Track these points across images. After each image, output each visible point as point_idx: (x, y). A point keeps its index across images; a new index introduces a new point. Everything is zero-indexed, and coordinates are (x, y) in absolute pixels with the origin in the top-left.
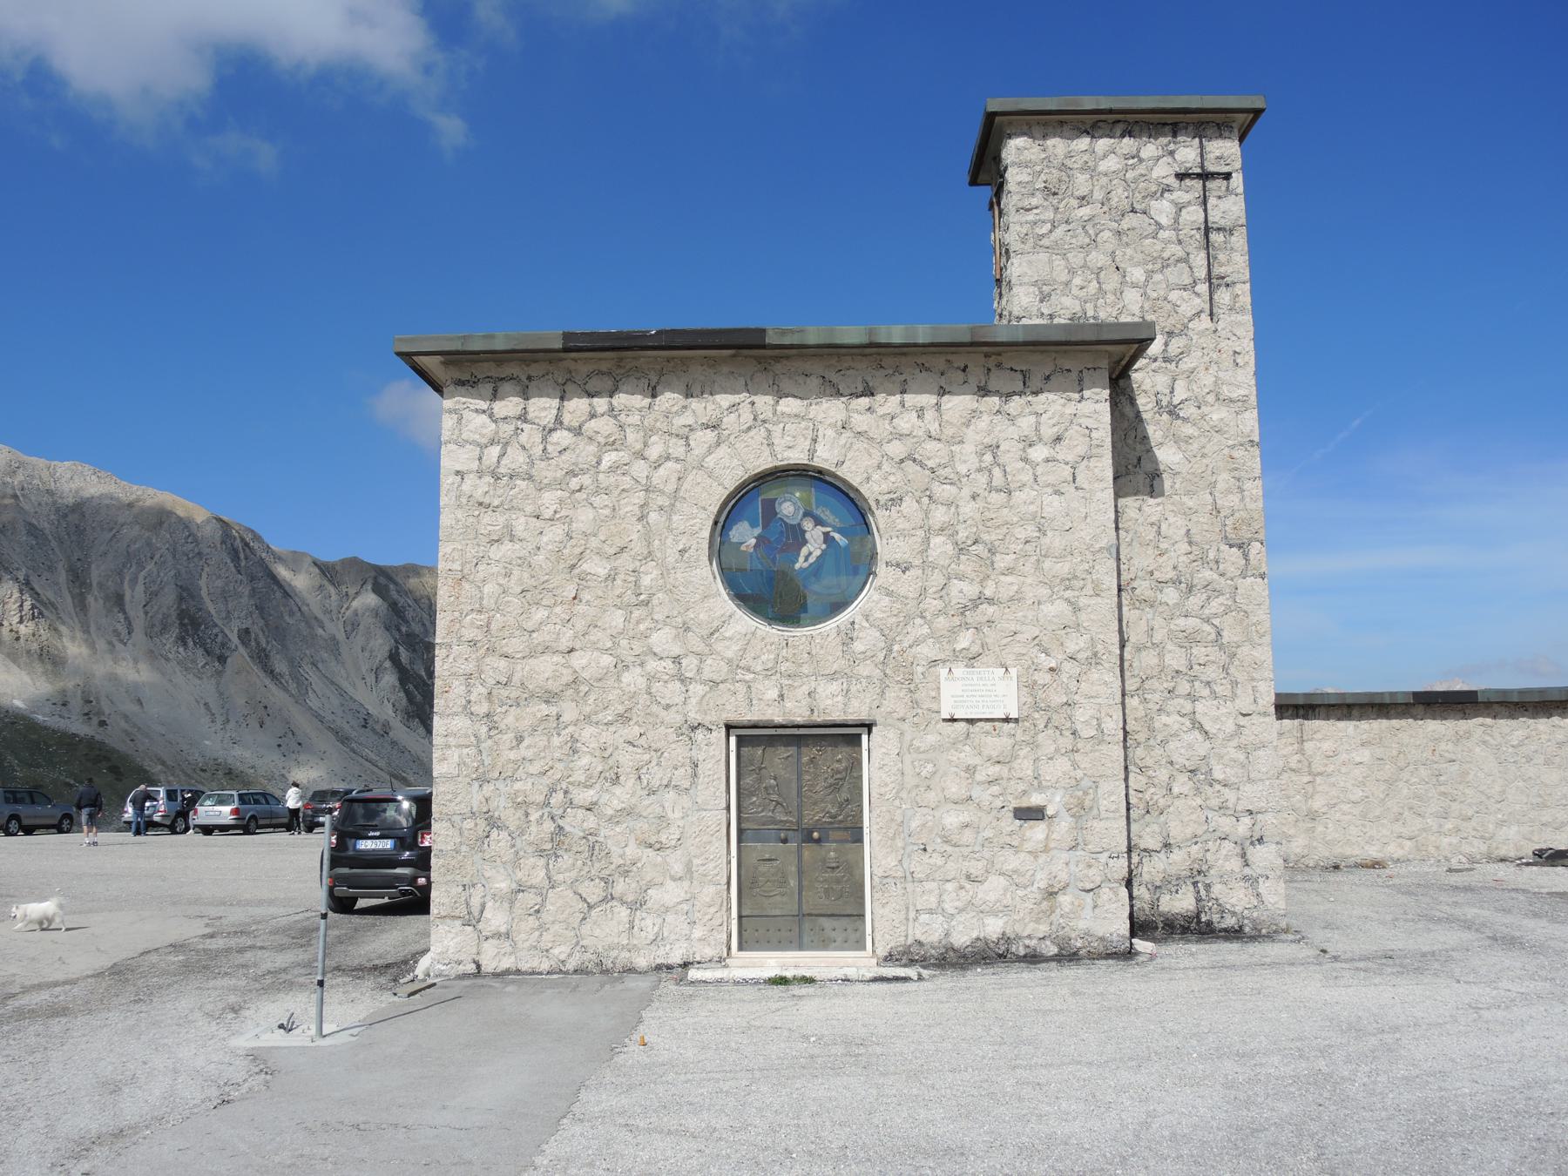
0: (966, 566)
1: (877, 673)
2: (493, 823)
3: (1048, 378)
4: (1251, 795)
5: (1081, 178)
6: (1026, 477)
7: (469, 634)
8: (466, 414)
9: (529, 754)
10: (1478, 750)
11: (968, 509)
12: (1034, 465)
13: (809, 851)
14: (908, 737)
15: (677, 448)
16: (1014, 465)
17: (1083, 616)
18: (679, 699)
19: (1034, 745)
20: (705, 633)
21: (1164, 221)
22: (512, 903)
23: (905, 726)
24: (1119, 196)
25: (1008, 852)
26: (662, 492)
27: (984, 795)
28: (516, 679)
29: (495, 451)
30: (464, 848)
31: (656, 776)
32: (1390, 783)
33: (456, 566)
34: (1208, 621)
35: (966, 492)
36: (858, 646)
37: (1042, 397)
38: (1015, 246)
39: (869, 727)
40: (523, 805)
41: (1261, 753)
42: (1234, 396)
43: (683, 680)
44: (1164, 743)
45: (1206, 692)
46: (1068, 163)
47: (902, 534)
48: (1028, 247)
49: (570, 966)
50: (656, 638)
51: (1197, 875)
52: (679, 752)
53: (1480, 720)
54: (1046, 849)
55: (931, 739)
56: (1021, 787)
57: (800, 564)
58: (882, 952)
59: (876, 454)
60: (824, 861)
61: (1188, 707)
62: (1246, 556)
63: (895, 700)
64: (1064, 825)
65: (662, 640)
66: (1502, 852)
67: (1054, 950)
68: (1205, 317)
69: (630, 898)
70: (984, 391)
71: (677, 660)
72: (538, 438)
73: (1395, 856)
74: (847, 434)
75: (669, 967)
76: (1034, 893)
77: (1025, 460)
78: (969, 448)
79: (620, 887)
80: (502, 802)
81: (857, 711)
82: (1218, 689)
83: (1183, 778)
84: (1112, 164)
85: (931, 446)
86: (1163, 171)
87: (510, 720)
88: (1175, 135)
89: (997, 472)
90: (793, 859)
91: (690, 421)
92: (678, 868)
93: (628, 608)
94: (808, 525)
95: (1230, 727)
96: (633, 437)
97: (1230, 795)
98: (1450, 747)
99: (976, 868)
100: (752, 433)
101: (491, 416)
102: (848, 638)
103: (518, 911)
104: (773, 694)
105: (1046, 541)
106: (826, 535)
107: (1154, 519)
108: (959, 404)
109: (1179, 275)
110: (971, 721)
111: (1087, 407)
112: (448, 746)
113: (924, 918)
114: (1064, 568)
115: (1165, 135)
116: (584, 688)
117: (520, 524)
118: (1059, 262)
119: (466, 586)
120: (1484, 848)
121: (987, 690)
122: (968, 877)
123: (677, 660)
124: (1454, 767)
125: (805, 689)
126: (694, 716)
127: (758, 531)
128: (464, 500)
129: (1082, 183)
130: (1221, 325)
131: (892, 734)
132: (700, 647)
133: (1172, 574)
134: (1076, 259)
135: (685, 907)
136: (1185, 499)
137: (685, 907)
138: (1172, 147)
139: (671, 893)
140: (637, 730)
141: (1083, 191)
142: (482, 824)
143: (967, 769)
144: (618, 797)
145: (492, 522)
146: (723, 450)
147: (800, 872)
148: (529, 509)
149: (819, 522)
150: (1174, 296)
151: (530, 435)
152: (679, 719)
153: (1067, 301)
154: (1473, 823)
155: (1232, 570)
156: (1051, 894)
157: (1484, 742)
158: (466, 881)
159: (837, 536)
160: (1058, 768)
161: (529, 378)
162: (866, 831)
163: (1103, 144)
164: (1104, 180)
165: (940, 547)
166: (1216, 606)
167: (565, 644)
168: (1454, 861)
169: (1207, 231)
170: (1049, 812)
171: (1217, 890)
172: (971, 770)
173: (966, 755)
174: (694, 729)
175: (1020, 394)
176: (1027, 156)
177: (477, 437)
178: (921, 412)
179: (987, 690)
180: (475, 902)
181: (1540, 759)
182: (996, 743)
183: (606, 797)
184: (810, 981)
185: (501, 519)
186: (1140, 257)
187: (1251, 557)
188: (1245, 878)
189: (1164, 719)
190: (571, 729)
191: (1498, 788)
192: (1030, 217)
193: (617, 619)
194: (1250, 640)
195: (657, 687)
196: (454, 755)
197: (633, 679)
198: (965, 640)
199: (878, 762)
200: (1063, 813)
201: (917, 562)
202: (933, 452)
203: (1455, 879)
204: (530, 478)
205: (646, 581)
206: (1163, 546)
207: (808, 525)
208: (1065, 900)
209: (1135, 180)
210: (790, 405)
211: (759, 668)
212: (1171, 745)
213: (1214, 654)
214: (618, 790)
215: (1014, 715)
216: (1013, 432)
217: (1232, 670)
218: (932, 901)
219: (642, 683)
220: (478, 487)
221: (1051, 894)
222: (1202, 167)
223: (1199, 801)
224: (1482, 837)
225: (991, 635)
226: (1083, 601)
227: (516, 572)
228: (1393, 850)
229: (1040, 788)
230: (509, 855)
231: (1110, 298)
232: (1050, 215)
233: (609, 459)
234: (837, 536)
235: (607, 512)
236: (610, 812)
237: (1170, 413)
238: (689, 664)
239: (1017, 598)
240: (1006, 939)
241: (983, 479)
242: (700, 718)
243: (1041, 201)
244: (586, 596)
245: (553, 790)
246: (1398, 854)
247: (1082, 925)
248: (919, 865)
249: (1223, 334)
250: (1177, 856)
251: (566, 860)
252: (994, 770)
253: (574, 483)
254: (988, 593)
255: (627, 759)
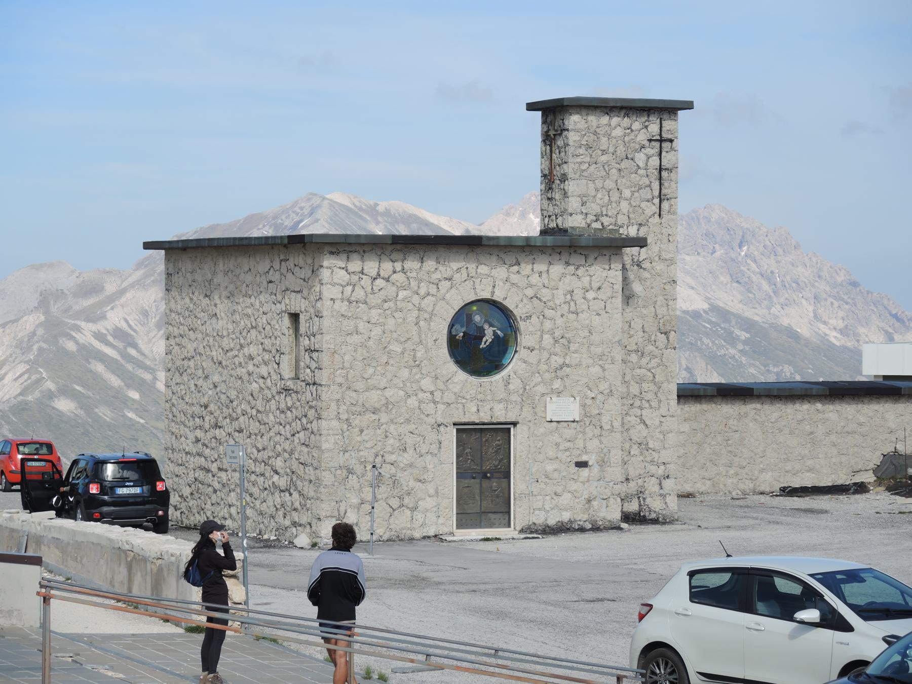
0: (558, 349)
1: (519, 399)
2: (350, 471)
3: (596, 259)
4: (665, 456)
5: (604, 140)
6: (585, 307)
7: (339, 380)
8: (335, 269)
9: (366, 438)
10: (751, 424)
11: (560, 321)
12: (588, 301)
13: (486, 483)
14: (532, 430)
15: (433, 290)
16: (580, 301)
17: (606, 373)
18: (433, 412)
19: (584, 433)
20: (445, 380)
21: (641, 165)
22: (358, 509)
23: (531, 424)
24: (621, 150)
25: (572, 482)
26: (426, 311)
27: (563, 456)
28: (360, 403)
29: (350, 288)
30: (336, 484)
31: (424, 448)
32: (700, 445)
33: (332, 346)
34: (649, 370)
35: (559, 313)
36: (511, 387)
37: (593, 268)
38: (571, 175)
39: (515, 424)
40: (364, 463)
41: (670, 435)
42: (667, 257)
43: (435, 402)
44: (628, 430)
45: (647, 405)
46: (598, 130)
47: (531, 333)
48: (577, 176)
49: (385, 537)
50: (423, 382)
51: (640, 494)
52: (432, 436)
53: (754, 406)
54: (588, 481)
55: (542, 430)
56: (579, 452)
57: (482, 346)
58: (518, 528)
59: (521, 294)
60: (491, 487)
61: (639, 412)
62: (668, 338)
63: (527, 413)
64: (596, 469)
65: (427, 384)
66: (762, 489)
67: (590, 526)
68: (657, 216)
69: (411, 506)
70: (568, 264)
71: (432, 393)
72: (369, 282)
73: (701, 490)
74: (508, 284)
75: (429, 537)
76: (582, 500)
77: (584, 298)
78: (561, 292)
79: (407, 501)
80: (354, 461)
81: (511, 418)
82: (653, 404)
83: (635, 447)
84: (618, 132)
85: (544, 291)
86: (642, 137)
87: (357, 422)
88: (648, 116)
89: (572, 304)
90: (478, 486)
91: (439, 277)
92: (432, 491)
93: (410, 368)
94: (486, 327)
95: (657, 423)
96: (414, 284)
97: (655, 455)
98: (735, 422)
99: (559, 489)
100: (467, 282)
101: (347, 271)
102: (507, 383)
103: (361, 513)
104: (474, 409)
105: (592, 337)
106: (494, 331)
107: (628, 319)
108: (557, 269)
109: (646, 194)
110: (558, 422)
111: (612, 273)
112: (329, 435)
113: (537, 512)
114: (599, 350)
115: (643, 116)
116: (391, 406)
117: (362, 326)
118: (591, 185)
119: (336, 356)
120: (751, 486)
121: (565, 408)
122: (555, 494)
123: (432, 393)
124: (737, 435)
125: (488, 407)
126: (440, 420)
127: (464, 329)
128: (335, 313)
129: (604, 143)
130: (663, 220)
131: (525, 428)
132: (442, 387)
133: (635, 347)
134: (599, 183)
135: (435, 509)
136: (643, 310)
137: (435, 509)
138: (647, 123)
139: (429, 503)
140: (414, 426)
141: (604, 147)
142: (345, 472)
143: (556, 444)
144: (406, 458)
145: (348, 325)
146: (453, 291)
147: (481, 493)
148: (365, 318)
149: (491, 325)
150: (644, 205)
151: (366, 281)
152: (433, 421)
153: (594, 206)
154: (746, 470)
155: (661, 346)
156: (589, 501)
157: (755, 420)
158: (338, 499)
159: (499, 332)
160: (593, 444)
161: (364, 251)
162: (512, 473)
163: (615, 120)
164: (614, 140)
165: (547, 340)
166: (654, 363)
167: (382, 385)
168: (734, 494)
169: (661, 170)
170: (590, 464)
171: (648, 500)
172: (557, 445)
173: (556, 438)
174: (439, 425)
175: (583, 266)
176: (579, 126)
177: (341, 282)
178: (540, 274)
179: (565, 408)
180: (342, 509)
181: (787, 431)
182: (569, 433)
183: (400, 458)
184: (499, 539)
185: (352, 323)
186: (628, 183)
187: (670, 339)
188: (661, 495)
189: (629, 418)
190: (384, 426)
191: (762, 449)
192: (579, 160)
193: (405, 373)
194: (667, 380)
195: (423, 406)
196: (332, 439)
197: (412, 402)
198: (557, 384)
199: (519, 440)
200: (596, 464)
201: (537, 347)
202: (545, 294)
203: (737, 502)
204: (366, 303)
205: (419, 355)
206: (632, 333)
207: (486, 327)
208: (595, 503)
209: (629, 142)
210: (483, 269)
211: (468, 397)
212: (631, 431)
213: (652, 387)
214: (405, 455)
215: (577, 419)
216: (579, 284)
217: (659, 395)
218: (540, 505)
219: (416, 404)
220: (342, 307)
221: (589, 501)
222: (660, 135)
223: (642, 458)
224: (751, 479)
225: (568, 382)
226: (607, 366)
227: (359, 349)
228: (700, 487)
229: (586, 453)
230: (357, 486)
231: (614, 205)
232: (588, 159)
233: (402, 294)
234: (499, 332)
235: (401, 320)
236: (402, 465)
237: (638, 265)
238: (438, 395)
239: (579, 365)
240: (570, 521)
241: (566, 307)
242: (442, 421)
243: (585, 152)
244: (391, 362)
245: (377, 455)
246: (703, 489)
247: (602, 515)
248: (535, 488)
249: (664, 224)
250: (632, 484)
251: (383, 488)
252: (568, 444)
253: (386, 305)
254: (567, 362)
255: (410, 440)
